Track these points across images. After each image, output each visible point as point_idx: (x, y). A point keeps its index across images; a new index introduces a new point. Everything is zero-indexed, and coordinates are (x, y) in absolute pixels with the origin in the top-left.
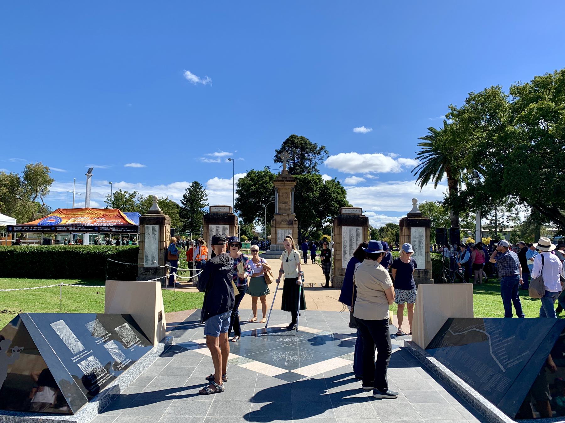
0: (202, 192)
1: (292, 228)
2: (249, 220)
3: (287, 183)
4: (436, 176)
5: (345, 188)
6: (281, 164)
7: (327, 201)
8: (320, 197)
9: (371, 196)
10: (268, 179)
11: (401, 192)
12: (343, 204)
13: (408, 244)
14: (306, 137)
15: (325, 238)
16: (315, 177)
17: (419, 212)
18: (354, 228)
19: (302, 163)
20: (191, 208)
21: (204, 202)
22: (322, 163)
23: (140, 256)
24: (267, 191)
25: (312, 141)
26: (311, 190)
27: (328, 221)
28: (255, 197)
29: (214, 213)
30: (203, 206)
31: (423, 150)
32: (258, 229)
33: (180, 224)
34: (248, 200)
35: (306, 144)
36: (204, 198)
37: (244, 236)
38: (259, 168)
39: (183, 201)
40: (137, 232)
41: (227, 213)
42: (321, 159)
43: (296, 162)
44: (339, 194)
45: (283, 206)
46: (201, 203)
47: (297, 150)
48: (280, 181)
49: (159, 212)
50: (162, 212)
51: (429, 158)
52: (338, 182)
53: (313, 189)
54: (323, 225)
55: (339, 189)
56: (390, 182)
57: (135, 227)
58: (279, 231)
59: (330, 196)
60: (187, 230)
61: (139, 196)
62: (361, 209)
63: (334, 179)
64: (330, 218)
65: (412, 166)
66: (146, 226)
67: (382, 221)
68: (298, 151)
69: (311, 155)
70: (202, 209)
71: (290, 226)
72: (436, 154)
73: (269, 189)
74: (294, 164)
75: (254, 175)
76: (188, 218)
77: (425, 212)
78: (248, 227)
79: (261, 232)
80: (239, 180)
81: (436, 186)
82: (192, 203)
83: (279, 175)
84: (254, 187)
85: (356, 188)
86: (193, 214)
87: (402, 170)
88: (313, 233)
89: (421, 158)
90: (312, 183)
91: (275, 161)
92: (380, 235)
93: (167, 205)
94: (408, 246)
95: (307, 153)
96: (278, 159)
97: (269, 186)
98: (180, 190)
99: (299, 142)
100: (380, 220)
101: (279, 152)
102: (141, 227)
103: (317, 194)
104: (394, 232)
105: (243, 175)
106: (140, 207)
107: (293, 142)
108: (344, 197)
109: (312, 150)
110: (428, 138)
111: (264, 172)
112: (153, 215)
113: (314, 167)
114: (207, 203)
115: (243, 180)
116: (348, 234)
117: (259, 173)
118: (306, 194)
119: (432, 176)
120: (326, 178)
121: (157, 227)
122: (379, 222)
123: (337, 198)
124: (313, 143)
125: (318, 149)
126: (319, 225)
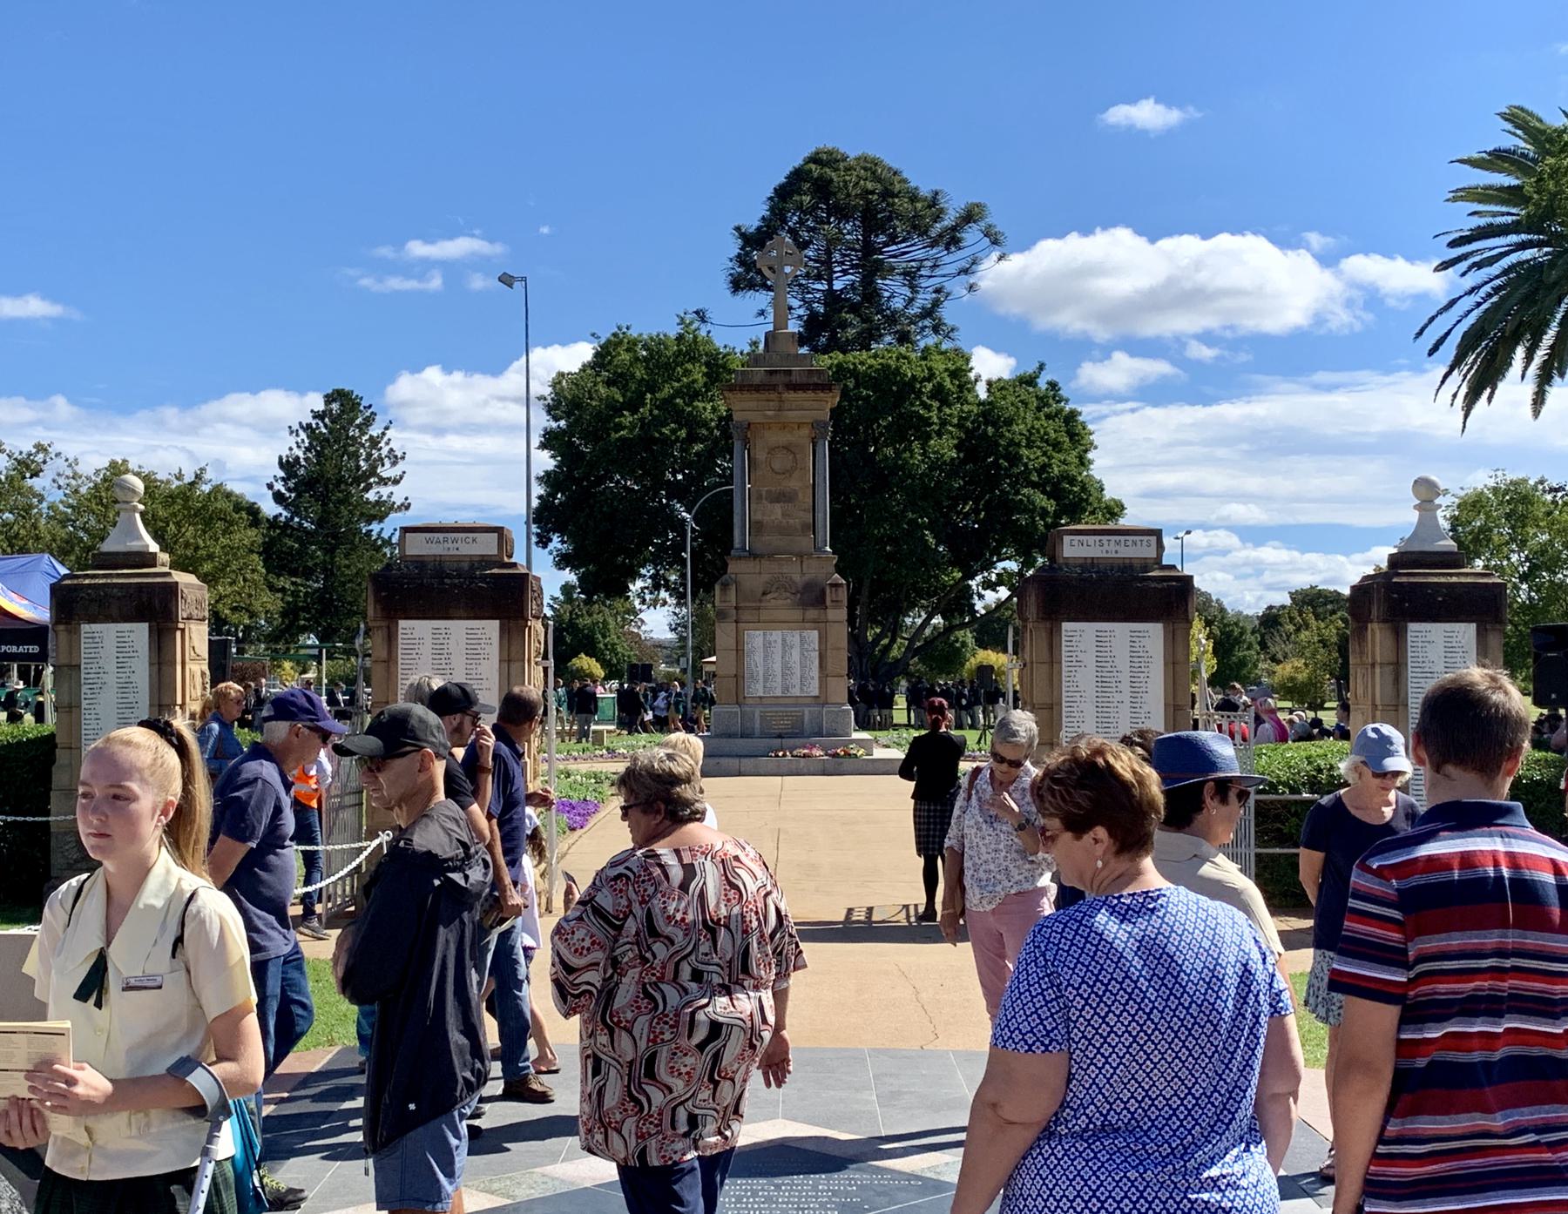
0: (374, 442)
1: (820, 624)
2: (603, 577)
3: (792, 395)
4: (1540, 355)
5: (1087, 412)
6: (762, 299)
7: (994, 482)
8: (963, 462)
9: (1221, 452)
10: (698, 374)
11: (1377, 428)
12: (1077, 500)
13: (1387, 729)
14: (891, 160)
15: (985, 671)
16: (939, 365)
17: (1449, 544)
18: (1120, 632)
19: (871, 295)
20: (320, 523)
21: (385, 491)
22: (971, 288)
23: (59, 778)
24: (692, 438)
26: (919, 429)
28: (631, 460)
29: (420, 562)
30: (381, 510)
31: (1482, 221)
32: (657, 621)
33: (269, 603)
34: (600, 480)
35: (887, 194)
36: (386, 471)
37: (585, 662)
38: (655, 321)
39: (279, 486)
40: (42, 657)
41: (486, 561)
42: (965, 271)
43: (838, 285)
44: (1057, 446)
45: (775, 513)
46: (371, 496)
47: (847, 225)
48: (758, 388)
49: (147, 559)
50: (164, 557)
51: (1506, 262)
52: (1053, 385)
53: (927, 422)
54: (979, 606)
55: (1059, 422)
56: (1321, 377)
57: (35, 633)
58: (755, 639)
59: (1015, 459)
60: (304, 629)
61: (60, 464)
62: (1157, 534)
63: (1030, 369)
64: (1012, 566)
65: (1421, 297)
66: (85, 627)
67: (1267, 577)
68: (851, 231)
69: (918, 251)
71: (812, 613)
72: (1539, 244)
73: (705, 424)
74: (832, 297)
75: (626, 357)
76: (308, 574)
77: (1485, 530)
78: (602, 613)
79: (671, 636)
80: (555, 384)
81: (1539, 400)
82: (324, 499)
83: (754, 359)
84: (627, 418)
85: (1151, 412)
86: (331, 551)
87: (1369, 317)
88: (929, 642)
89: (1464, 265)
91: (737, 285)
92: (1263, 645)
93: (190, 512)
94: (1385, 741)
95: (893, 240)
96: (746, 278)
97: (705, 409)
98: (265, 428)
99: (851, 184)
100: (1258, 569)
101: (753, 241)
102: (63, 636)
103: (945, 447)
104: (1331, 633)
105: (576, 356)
106: (63, 522)
107: (823, 189)
108: (1083, 462)
109: (918, 227)
110: (1498, 159)
111: (680, 338)
112: (125, 576)
113: (928, 313)
114: (398, 500)
115: (576, 380)
116: (1090, 659)
117: (655, 347)
118: (889, 451)
119: (1520, 352)
120: (989, 366)
121: (139, 632)
122: (1251, 582)
123: (1044, 468)
124: (925, 191)
125: (948, 221)
126: (957, 603)
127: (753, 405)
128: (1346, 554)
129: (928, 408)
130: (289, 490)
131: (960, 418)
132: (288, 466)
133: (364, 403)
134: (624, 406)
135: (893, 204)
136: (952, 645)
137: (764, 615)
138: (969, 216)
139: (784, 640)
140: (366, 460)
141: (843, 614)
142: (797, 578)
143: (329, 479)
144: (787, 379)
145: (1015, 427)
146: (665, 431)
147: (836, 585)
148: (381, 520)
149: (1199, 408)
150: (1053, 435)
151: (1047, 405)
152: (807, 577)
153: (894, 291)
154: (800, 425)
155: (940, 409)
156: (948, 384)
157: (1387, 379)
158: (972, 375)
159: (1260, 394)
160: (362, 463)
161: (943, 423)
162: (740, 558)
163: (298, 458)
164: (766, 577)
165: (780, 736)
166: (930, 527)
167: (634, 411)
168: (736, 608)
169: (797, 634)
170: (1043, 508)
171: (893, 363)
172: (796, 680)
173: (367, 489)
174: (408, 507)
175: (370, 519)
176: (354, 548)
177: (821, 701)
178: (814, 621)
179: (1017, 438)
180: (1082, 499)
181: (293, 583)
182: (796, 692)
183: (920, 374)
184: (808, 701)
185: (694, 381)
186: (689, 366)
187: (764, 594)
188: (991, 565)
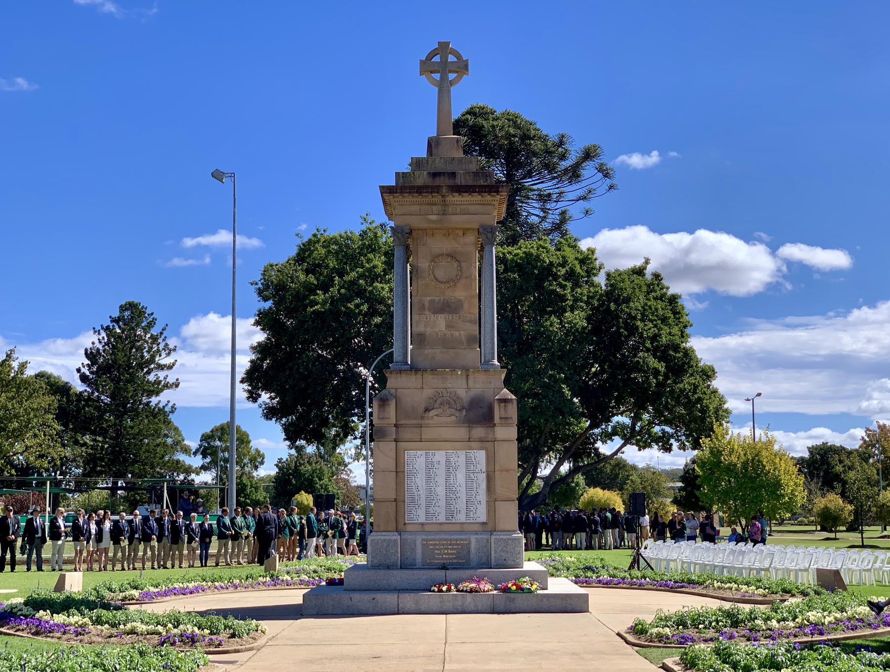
0: (154, 339)
3: (456, 198)
11: (823, 352)
21: (161, 375)
24: (372, 312)
25: (548, 127)
26: (554, 304)
27: (615, 433)
30: (157, 388)
35: (525, 137)
39: (86, 371)
42: (584, 198)
44: (664, 320)
45: (439, 324)
46: (151, 378)
48: (419, 190)
53: (563, 298)
56: (790, 320)
59: (632, 330)
64: (624, 420)
69: (547, 186)
70: (154, 400)
71: (479, 432)
82: (116, 381)
84: (320, 296)
90: (556, 277)
95: (529, 174)
103: (578, 318)
111: (363, 234)
123: (655, 338)
127: (415, 208)
128: (795, 433)
129: (564, 287)
130: (92, 373)
131: (588, 297)
132: (91, 355)
133: (148, 311)
134: (318, 287)
135: (530, 145)
136: (568, 485)
137: (427, 433)
138: (588, 155)
139: (448, 461)
140: (148, 352)
141: (512, 432)
142: (462, 393)
143: (120, 365)
144: (451, 182)
145: (631, 304)
146: (351, 306)
147: (505, 401)
148: (157, 394)
149: (710, 339)
150: (661, 312)
151: (654, 291)
152: (473, 393)
153: (531, 211)
154: (465, 231)
155: (572, 290)
156: (578, 269)
157: (828, 322)
158: (597, 263)
159: (752, 330)
160: (145, 354)
161: (576, 300)
162: (400, 371)
163: (98, 350)
164: (428, 392)
165: (444, 567)
166: (566, 381)
167: (326, 290)
168: (396, 426)
169: (462, 454)
170: (655, 368)
171: (534, 251)
172: (461, 505)
173: (148, 373)
174: (177, 386)
175: (150, 393)
176: (138, 414)
177: (489, 528)
178: (481, 440)
179: (633, 313)
180: (684, 363)
181: (95, 440)
182: (461, 518)
183: (554, 259)
184: (477, 528)
185: (374, 267)
186: (371, 256)
187: (427, 410)
188: (608, 420)
